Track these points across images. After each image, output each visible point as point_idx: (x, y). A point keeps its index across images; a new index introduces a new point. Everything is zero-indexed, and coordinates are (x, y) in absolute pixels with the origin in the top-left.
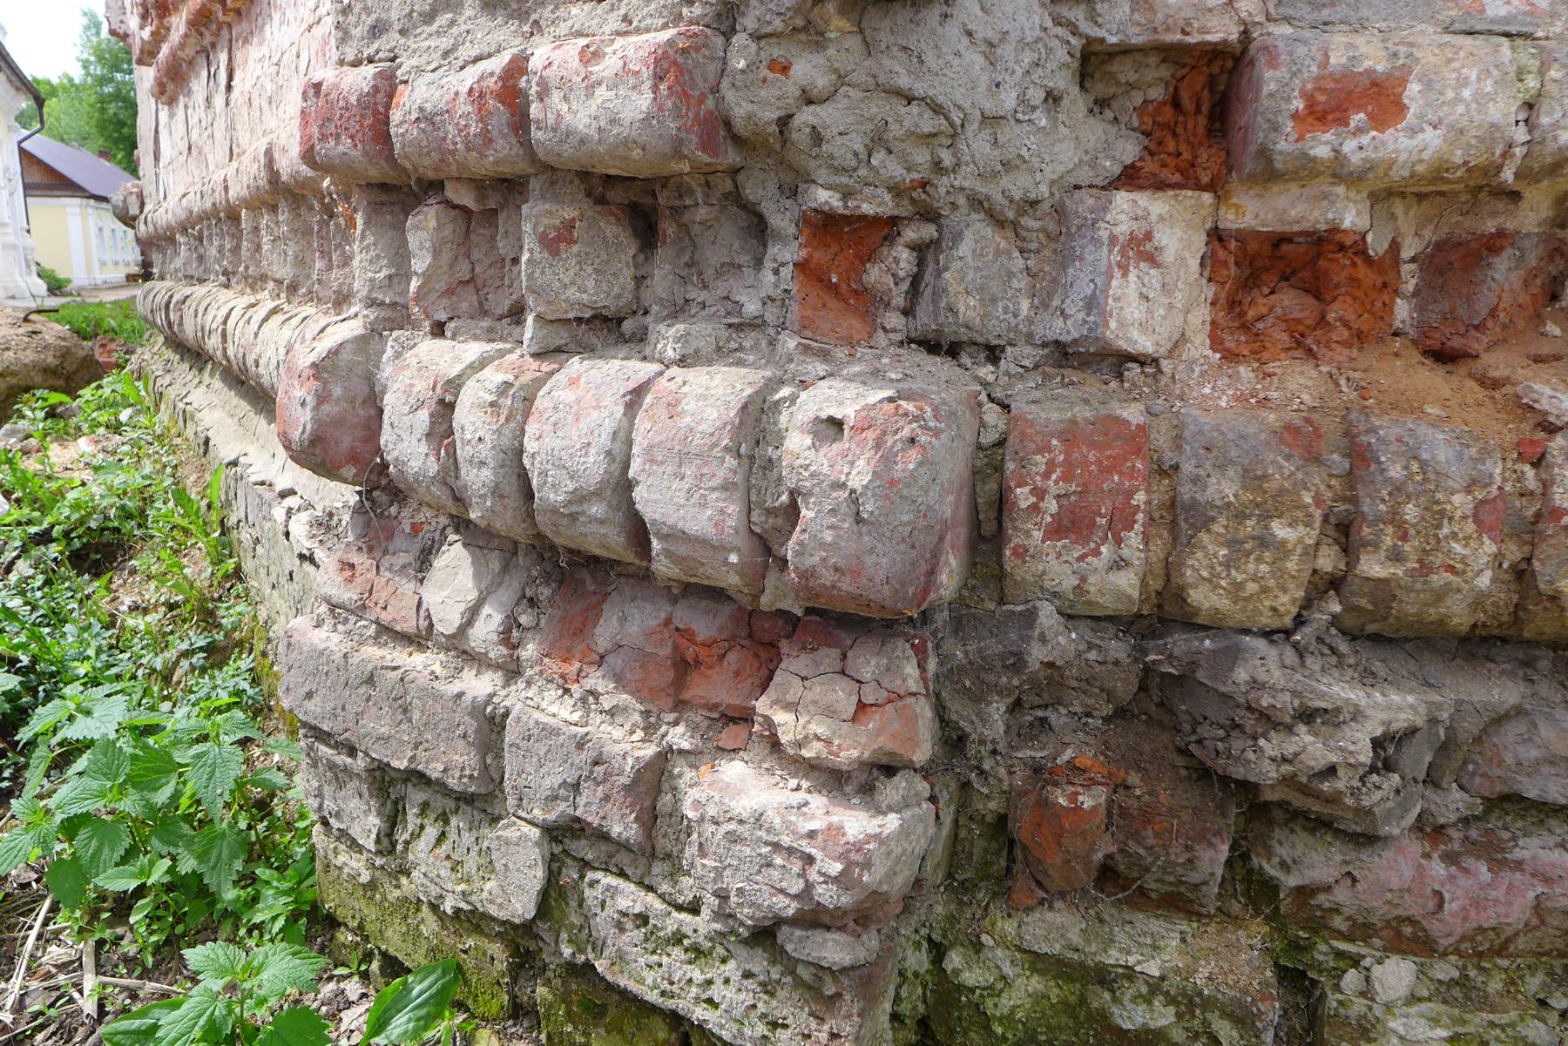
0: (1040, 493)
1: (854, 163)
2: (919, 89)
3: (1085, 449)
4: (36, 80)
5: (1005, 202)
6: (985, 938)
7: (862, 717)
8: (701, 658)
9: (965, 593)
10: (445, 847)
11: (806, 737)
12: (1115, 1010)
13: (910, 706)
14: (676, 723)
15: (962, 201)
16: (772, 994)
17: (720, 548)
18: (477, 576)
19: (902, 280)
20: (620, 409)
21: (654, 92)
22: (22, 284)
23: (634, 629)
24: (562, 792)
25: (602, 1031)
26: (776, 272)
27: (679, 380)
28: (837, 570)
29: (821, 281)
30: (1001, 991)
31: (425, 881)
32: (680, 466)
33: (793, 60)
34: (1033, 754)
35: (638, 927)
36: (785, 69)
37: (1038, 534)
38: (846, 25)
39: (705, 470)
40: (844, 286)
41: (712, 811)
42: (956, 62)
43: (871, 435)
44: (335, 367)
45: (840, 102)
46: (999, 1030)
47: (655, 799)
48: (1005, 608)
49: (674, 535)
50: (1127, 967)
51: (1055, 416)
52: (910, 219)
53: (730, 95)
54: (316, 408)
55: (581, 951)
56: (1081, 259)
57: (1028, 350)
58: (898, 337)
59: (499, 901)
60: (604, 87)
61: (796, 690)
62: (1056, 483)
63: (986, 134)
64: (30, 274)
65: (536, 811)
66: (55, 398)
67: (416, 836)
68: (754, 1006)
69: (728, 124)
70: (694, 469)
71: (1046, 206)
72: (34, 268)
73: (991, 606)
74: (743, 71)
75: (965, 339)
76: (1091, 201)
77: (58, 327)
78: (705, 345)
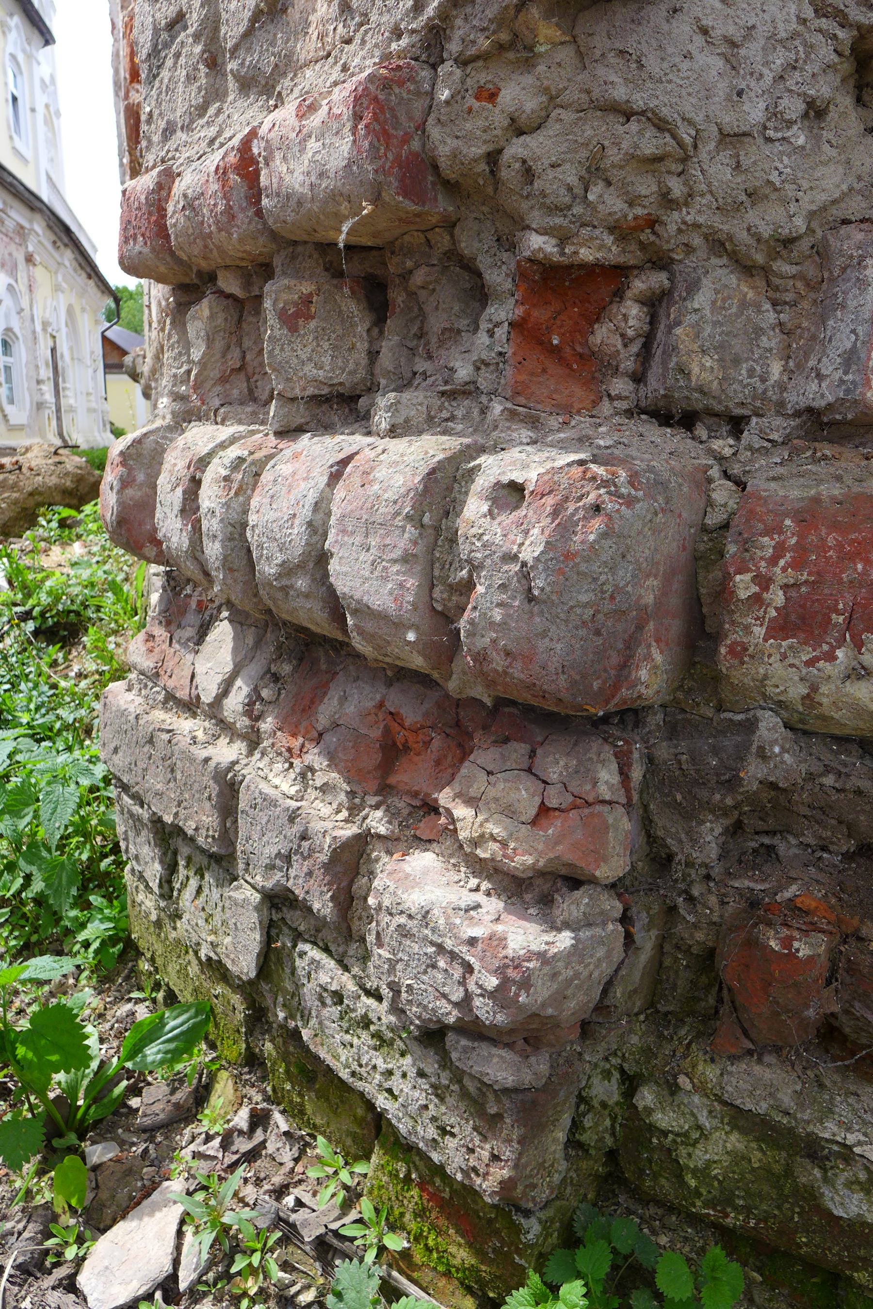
0: (764, 582)
1: (567, 200)
2: (639, 101)
3: (824, 531)
4: (117, 288)
5: (752, 242)
6: (683, 1080)
7: (543, 821)
8: (410, 744)
9: (680, 695)
10: (202, 899)
11: (482, 836)
12: (826, 1191)
13: (600, 814)
14: (377, 807)
15: (697, 241)
16: (442, 1099)
17: (400, 626)
18: (235, 650)
19: (632, 340)
20: (325, 479)
21: (354, 134)
22: (99, 438)
23: (350, 709)
24: (278, 862)
25: (313, 1094)
26: (491, 333)
27: (379, 450)
28: (508, 654)
29: (541, 343)
30: (697, 1141)
31: (189, 928)
32: (367, 536)
33: (501, 84)
34: (752, 885)
35: (335, 1004)
36: (492, 97)
37: (759, 631)
38: (557, 34)
39: (388, 541)
40: (568, 349)
41: (386, 903)
42: (685, 65)
43: (550, 501)
44: (140, 455)
45: (552, 128)
46: (693, 1183)
47: (351, 883)
48: (724, 715)
49: (363, 611)
50: (845, 1145)
51: (795, 493)
52: (640, 268)
53: (435, 132)
54: (120, 492)
55: (292, 1016)
56: (844, 307)
57: (779, 421)
58: (623, 405)
59: (232, 956)
60: (313, 139)
61: (479, 785)
62: (784, 569)
63: (725, 155)
64: (105, 431)
65: (258, 878)
66: (66, 512)
67: (184, 885)
68: (426, 1107)
69: (436, 167)
70: (378, 539)
71: (805, 245)
72: (108, 426)
73: (709, 713)
74: (447, 102)
75: (699, 406)
76: (860, 236)
77: (77, 459)
78: (417, 414)
